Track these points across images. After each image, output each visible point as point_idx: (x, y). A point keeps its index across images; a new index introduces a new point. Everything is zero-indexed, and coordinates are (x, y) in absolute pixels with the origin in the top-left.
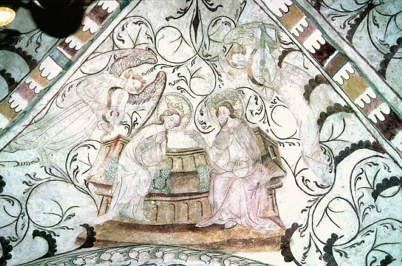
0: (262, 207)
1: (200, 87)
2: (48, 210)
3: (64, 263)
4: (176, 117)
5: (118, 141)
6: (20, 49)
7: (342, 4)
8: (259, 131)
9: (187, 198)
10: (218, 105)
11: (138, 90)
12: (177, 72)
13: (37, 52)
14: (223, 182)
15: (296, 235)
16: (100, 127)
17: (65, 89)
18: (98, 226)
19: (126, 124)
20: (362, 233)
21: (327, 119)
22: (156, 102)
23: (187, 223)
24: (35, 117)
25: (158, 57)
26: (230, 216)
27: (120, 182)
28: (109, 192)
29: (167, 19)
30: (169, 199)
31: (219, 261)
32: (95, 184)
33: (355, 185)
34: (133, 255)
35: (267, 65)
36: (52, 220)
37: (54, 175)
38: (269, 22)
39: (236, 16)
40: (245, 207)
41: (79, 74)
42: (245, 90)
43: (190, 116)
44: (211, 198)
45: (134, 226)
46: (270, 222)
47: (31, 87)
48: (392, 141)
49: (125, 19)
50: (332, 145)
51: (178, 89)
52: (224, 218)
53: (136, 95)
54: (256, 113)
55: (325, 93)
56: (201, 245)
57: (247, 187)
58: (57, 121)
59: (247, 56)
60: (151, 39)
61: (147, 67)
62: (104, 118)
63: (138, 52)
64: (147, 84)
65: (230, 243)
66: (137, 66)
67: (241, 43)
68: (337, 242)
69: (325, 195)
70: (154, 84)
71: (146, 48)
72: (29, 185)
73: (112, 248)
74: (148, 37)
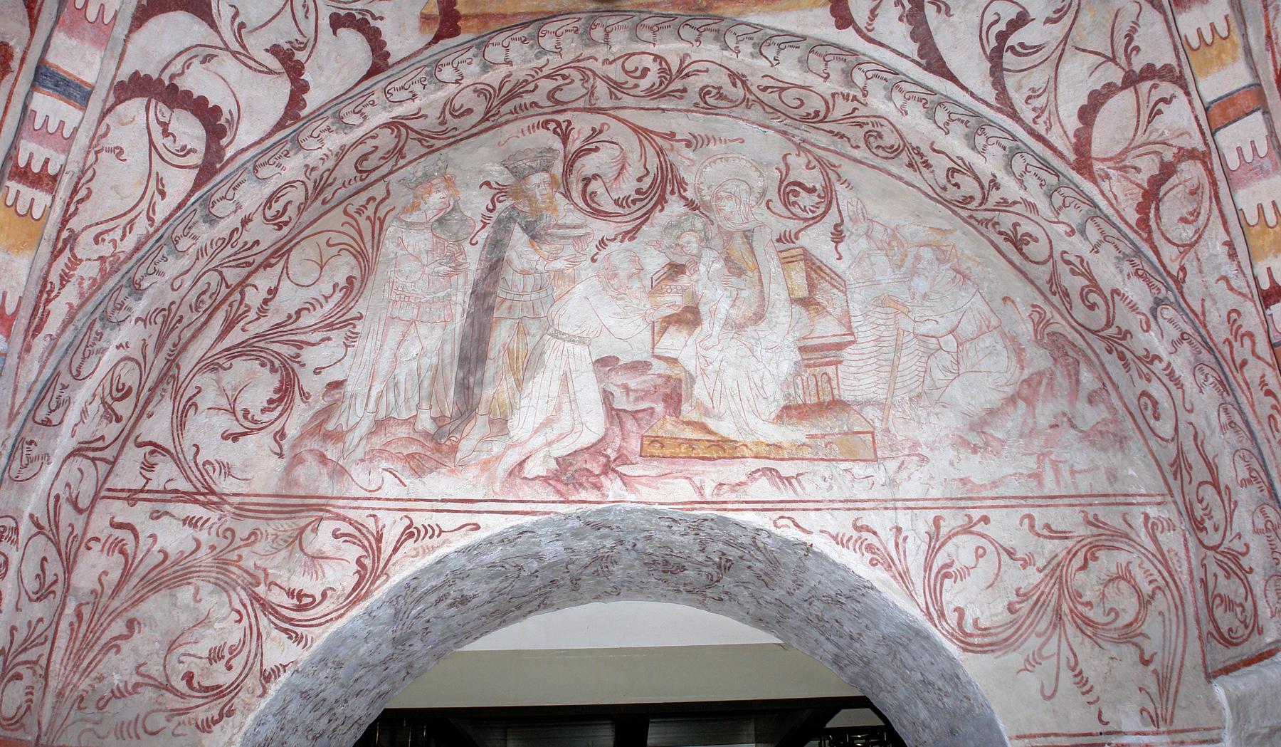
3: (420, 81)
31: (716, 39)
34: (548, 43)
73: (501, 31)
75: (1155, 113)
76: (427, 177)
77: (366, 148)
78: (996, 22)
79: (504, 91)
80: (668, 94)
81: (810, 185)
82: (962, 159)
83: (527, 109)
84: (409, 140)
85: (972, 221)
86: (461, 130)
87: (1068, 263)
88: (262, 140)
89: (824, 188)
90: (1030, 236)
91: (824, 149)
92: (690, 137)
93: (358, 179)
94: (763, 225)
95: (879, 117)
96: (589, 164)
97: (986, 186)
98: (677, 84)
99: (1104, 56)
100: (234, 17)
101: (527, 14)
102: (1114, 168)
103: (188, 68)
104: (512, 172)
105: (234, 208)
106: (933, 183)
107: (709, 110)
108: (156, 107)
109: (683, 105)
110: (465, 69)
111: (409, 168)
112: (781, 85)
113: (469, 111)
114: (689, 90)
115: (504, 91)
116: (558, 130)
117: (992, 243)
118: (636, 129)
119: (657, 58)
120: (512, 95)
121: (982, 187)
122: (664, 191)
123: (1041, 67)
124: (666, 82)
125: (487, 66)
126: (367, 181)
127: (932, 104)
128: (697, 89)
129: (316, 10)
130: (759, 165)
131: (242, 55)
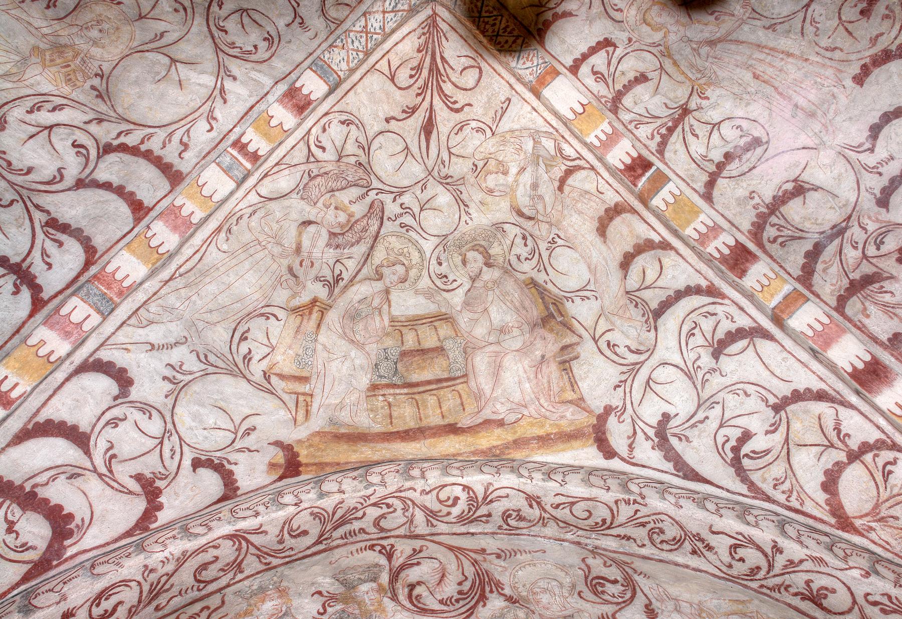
0: (556, 389)
1: (433, 222)
2: (211, 422)
4: (400, 269)
7: (649, 107)
8: (533, 283)
9: (434, 386)
10: (464, 249)
11: (342, 227)
12: (399, 201)
13: (182, 158)
14: (486, 360)
15: (612, 421)
16: (284, 284)
17: (230, 221)
18: (299, 442)
20: (703, 407)
21: (635, 260)
23: (442, 423)
24: (180, 267)
25: (372, 177)
26: (509, 406)
27: (323, 372)
28: (307, 388)
29: (387, 120)
30: (405, 391)
32: (281, 376)
33: (687, 344)
35: (542, 190)
36: (218, 439)
37: (212, 365)
38: (544, 129)
39: (494, 121)
40: (529, 390)
41: (253, 198)
42: (506, 226)
44: (472, 384)
45: (357, 437)
46: (572, 408)
48: (744, 279)
49: (326, 114)
50: (646, 294)
52: (501, 410)
54: (526, 259)
55: (629, 225)
56: (474, 453)
57: (526, 362)
58: (216, 274)
59: (510, 179)
60: (364, 149)
61: (355, 192)
62: (290, 270)
63: (343, 168)
65: (518, 443)
66: (343, 189)
67: (501, 159)
68: (673, 423)
69: (643, 363)
72: (174, 383)
73: (335, 473)
75: (886, 475)
76: (262, 589)
77: (208, 557)
78: (727, 441)
79: (337, 516)
80: (476, 520)
81: (613, 578)
82: (741, 534)
83: (355, 535)
84: (249, 556)
85: (765, 590)
86: (296, 551)
87: (875, 604)
88: (108, 544)
89: (625, 579)
90: (826, 589)
91: (615, 552)
92: (499, 551)
93: (195, 588)
94: (579, 611)
95: (659, 514)
96: (413, 575)
97: (770, 553)
98: (483, 510)
99: (823, 445)
100: (108, 450)
101: (357, 462)
102: (874, 521)
103: (54, 480)
104: (342, 584)
105: (58, 599)
106: (718, 564)
107: (513, 531)
108: (8, 508)
109: (489, 528)
110: (303, 497)
111: (246, 582)
112: (571, 500)
113: (305, 533)
114: (494, 514)
115: (337, 516)
116: (384, 551)
117: (789, 605)
118: (451, 548)
119: (466, 488)
120: (343, 522)
121: (766, 555)
122: (483, 590)
123: (776, 463)
124: (474, 509)
125: (322, 495)
126: (204, 592)
127: (701, 501)
128: (500, 514)
129: (182, 454)
130: (563, 567)
131: (107, 477)
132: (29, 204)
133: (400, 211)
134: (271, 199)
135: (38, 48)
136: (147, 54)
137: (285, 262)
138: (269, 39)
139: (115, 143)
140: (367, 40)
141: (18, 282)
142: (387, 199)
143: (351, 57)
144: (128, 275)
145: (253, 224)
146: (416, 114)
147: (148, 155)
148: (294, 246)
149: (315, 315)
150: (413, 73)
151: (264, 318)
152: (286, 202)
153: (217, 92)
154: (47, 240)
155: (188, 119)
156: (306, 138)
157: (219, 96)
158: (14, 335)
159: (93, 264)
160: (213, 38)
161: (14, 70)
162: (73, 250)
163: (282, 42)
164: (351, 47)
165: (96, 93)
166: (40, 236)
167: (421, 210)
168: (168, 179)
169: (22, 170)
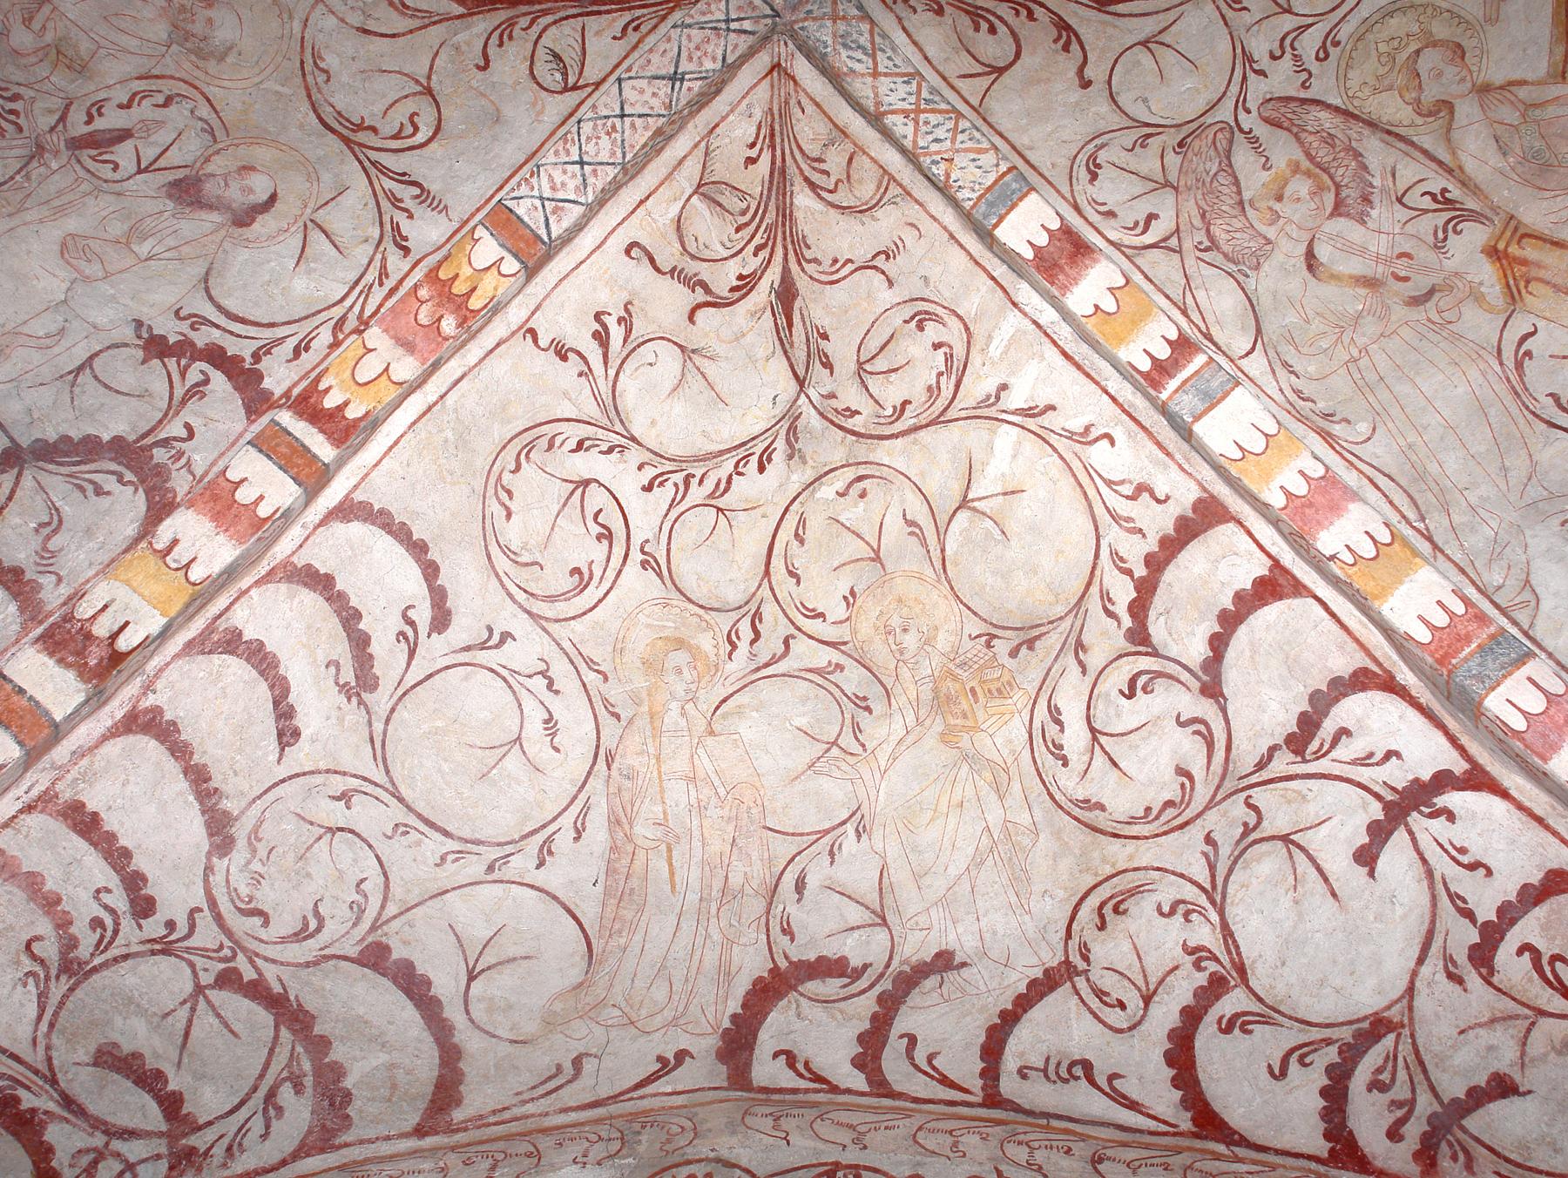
5: (1506, 255)
6: (1149, 560)
11: (1320, 189)
12: (1264, 63)
13: (1168, 498)
19: (1445, 231)
22: (1366, 131)
24: (1404, 517)
25: (1209, 120)
29: (1086, 84)
43: (1429, 11)
47: (1300, 488)
49: (1076, 208)
51: (1327, 56)
53: (1337, 195)
61: (1243, 158)
64: (1301, 154)
66: (1237, 183)
70: (1303, 135)
71: (1178, 153)
74: (1143, 146)
132: (1254, 779)
133: (1287, 62)
134: (1259, 331)
135: (942, 734)
136: (948, 552)
137: (1400, 312)
138: (920, 321)
139: (1127, 622)
140: (933, 111)
141: (1427, 810)
142: (1258, 89)
143: (969, 144)
144: (1439, 603)
145: (1311, 369)
146: (1072, 21)
147: (1157, 563)
148: (1363, 291)
149: (1530, 251)
150: (984, 26)
151: (1527, 361)
152: (1265, 302)
153: (1030, 423)
154: (1333, 754)
155: (1085, 482)
156: (1128, 251)
157: (1039, 420)
158: (1547, 827)
159: (1392, 678)
160: (916, 429)
161: (988, 775)
162: (1359, 711)
163: (926, 294)
164: (948, 143)
165: (1024, 650)
166: (1323, 766)
167: (1289, 11)
168: (1210, 526)
169: (1183, 785)
